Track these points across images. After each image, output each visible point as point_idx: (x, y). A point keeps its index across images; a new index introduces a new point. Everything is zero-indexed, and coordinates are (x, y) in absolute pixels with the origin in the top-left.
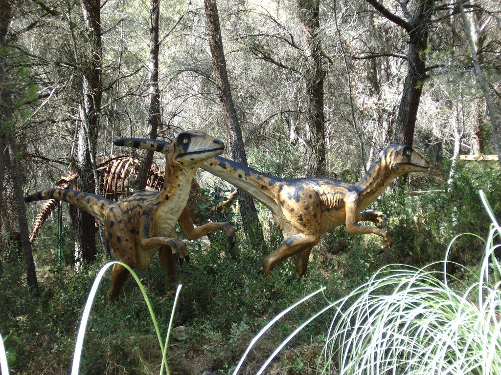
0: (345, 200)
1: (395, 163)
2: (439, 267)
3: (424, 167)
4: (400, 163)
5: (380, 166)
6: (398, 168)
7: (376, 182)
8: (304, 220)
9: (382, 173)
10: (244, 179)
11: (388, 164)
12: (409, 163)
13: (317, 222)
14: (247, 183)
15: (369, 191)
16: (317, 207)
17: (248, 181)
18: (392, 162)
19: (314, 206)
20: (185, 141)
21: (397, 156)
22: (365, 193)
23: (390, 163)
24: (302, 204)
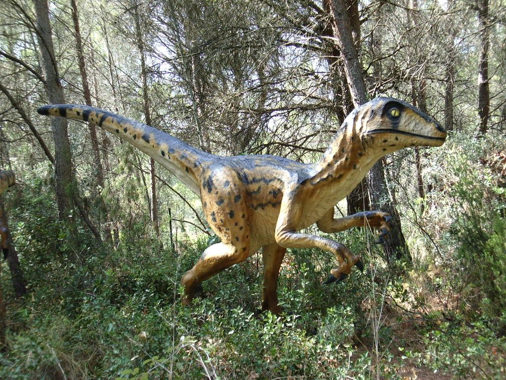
0: (283, 191)
1: (368, 129)
2: (73, 323)
3: (430, 138)
4: (375, 130)
5: (345, 136)
6: (372, 138)
7: (339, 163)
8: (217, 220)
9: (349, 146)
10: (167, 157)
11: (358, 131)
12: (395, 130)
13: (236, 224)
14: (170, 163)
15: (325, 176)
16: (236, 201)
17: (171, 160)
18: (363, 130)
19: (230, 199)
20: (394, 112)
21: (373, 118)
22: (318, 180)
23: (361, 130)
24: (214, 195)
